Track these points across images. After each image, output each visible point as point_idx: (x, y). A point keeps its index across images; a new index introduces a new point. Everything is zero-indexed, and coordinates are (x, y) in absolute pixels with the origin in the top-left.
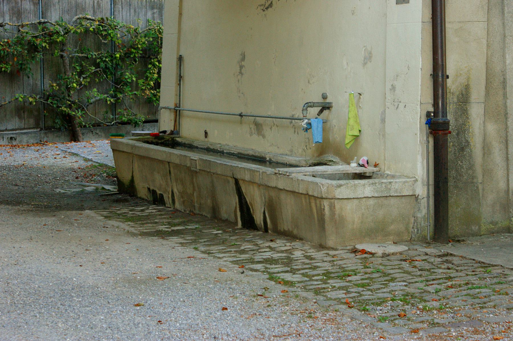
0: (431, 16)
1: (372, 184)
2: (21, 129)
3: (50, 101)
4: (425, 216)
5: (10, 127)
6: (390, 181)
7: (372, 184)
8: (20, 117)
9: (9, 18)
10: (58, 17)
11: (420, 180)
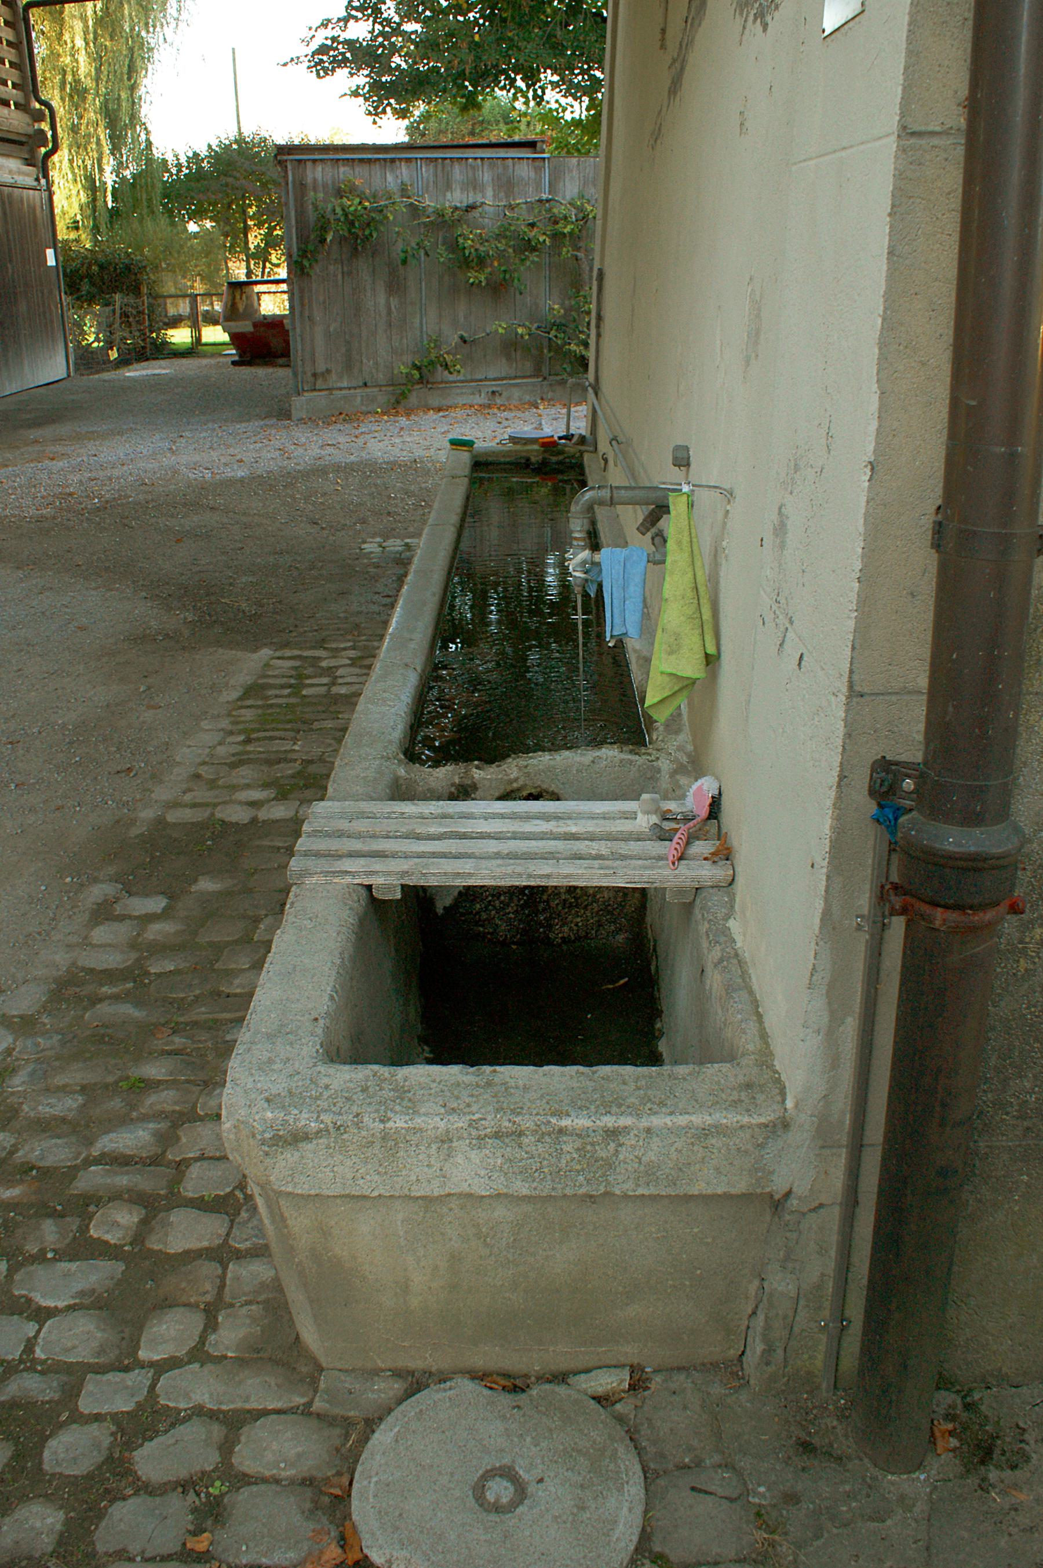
0: (964, 92)
1: (497, 1135)
2: (510, 378)
3: (553, 333)
4: (819, 1287)
5: (491, 376)
6: (609, 1121)
7: (497, 1135)
8: (509, 358)
9: (492, 193)
10: (576, 190)
11: (805, 1120)
